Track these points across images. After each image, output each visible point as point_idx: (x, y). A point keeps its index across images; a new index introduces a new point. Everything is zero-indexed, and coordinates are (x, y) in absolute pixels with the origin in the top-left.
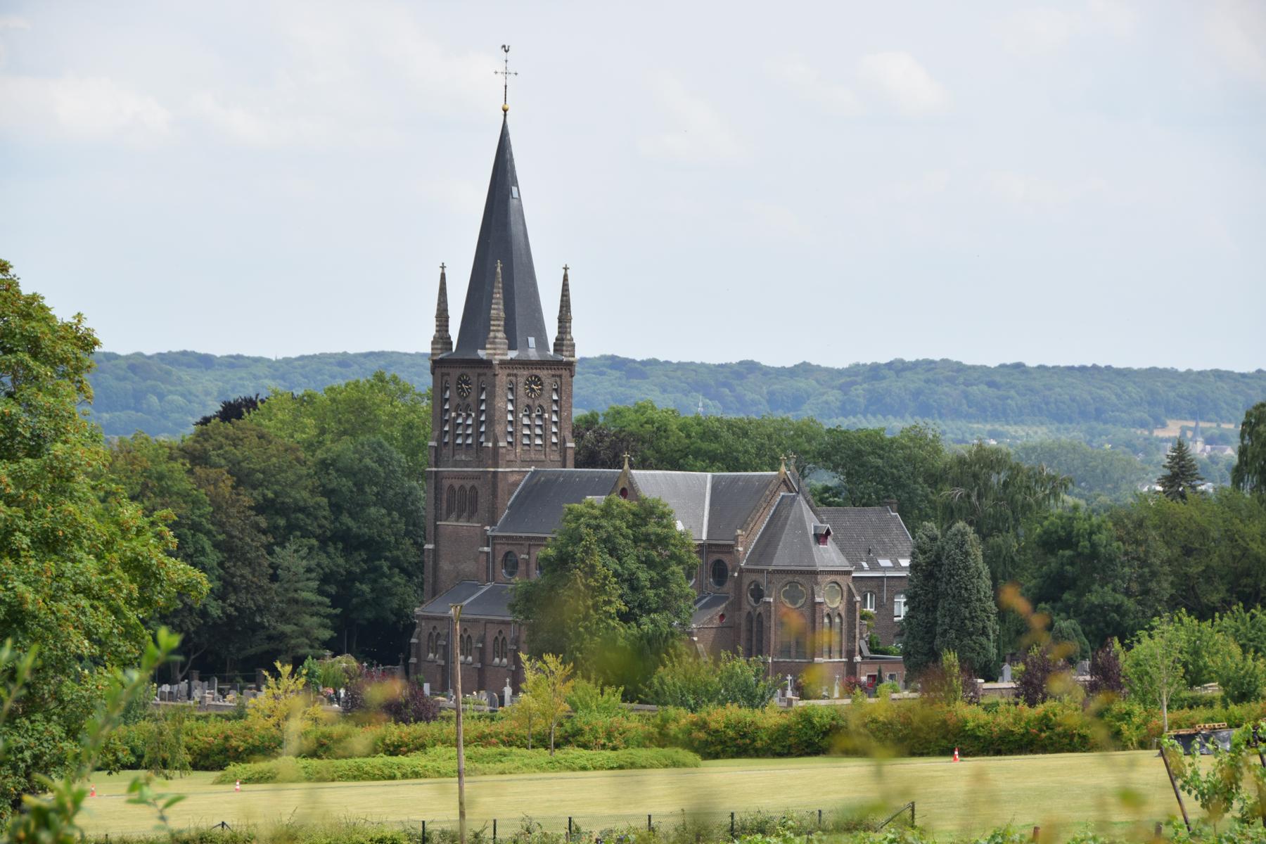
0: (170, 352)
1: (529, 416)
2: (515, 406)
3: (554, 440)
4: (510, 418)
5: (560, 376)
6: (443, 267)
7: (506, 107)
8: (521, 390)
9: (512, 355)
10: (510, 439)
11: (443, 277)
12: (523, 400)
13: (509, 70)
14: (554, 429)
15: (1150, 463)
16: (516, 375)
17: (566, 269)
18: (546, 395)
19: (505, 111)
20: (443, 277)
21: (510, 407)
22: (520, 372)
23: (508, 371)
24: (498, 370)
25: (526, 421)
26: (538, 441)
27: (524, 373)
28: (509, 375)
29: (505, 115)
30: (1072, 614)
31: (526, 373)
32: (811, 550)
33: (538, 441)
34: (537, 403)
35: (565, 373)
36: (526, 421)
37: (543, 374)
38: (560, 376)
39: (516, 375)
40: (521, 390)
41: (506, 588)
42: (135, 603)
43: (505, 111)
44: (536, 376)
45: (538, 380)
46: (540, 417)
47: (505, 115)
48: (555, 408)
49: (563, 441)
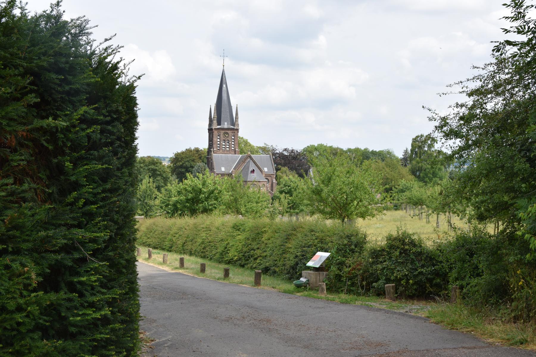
0: (137, 124)
1: (225, 142)
2: (220, 140)
3: (233, 149)
4: (218, 143)
8: (222, 136)
9: (219, 127)
10: (218, 148)
12: (222, 138)
13: (223, 57)
14: (233, 146)
15: (451, 264)
20: (237, 107)
21: (218, 140)
22: (221, 131)
24: (214, 131)
26: (228, 149)
30: (48, 289)
31: (223, 131)
32: (248, 175)
33: (228, 149)
34: (227, 139)
35: (236, 132)
36: (224, 144)
37: (229, 132)
40: (222, 136)
41: (19, 165)
42: (293, 190)
45: (227, 133)
46: (228, 143)
48: (233, 140)
49: (235, 149)
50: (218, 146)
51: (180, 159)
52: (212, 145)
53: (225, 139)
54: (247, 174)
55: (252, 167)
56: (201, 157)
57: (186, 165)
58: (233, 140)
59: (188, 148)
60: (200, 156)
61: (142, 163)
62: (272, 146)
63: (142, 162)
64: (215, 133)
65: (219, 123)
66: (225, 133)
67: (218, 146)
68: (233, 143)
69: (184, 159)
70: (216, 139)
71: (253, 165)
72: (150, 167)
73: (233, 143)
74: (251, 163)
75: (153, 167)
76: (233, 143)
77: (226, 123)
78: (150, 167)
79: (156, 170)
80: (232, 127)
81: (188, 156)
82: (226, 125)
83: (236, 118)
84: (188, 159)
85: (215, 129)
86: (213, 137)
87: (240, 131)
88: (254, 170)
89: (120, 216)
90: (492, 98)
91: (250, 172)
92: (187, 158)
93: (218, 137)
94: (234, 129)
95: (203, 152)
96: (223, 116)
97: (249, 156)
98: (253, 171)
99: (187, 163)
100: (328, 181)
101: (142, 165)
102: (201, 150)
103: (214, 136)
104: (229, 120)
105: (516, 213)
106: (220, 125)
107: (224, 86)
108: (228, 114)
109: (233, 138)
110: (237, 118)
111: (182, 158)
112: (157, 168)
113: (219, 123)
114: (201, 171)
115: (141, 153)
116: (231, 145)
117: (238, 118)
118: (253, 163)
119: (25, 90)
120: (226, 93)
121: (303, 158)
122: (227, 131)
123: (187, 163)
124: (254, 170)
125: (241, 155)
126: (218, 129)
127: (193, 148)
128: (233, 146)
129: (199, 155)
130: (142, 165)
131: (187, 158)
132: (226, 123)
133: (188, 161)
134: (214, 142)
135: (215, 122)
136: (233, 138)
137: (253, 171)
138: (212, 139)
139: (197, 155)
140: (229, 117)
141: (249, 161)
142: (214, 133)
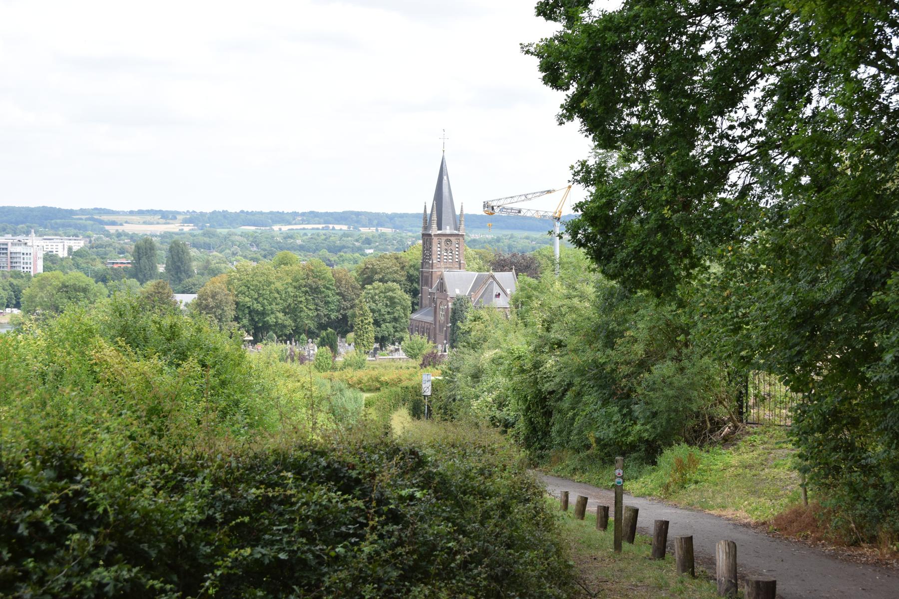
8: (443, 244)
9: (439, 232)
12: (444, 247)
18: (453, 245)
21: (439, 249)
24: (433, 237)
25: (445, 254)
27: (445, 238)
36: (445, 254)
37: (452, 238)
40: (443, 244)
45: (450, 241)
54: (491, 299)
55: (496, 290)
64: (435, 240)
65: (440, 228)
70: (435, 248)
71: (498, 287)
75: (390, 294)
76: (457, 253)
77: (448, 227)
79: (394, 298)
80: (456, 232)
82: (448, 230)
85: (435, 235)
88: (499, 294)
90: (835, 298)
91: (494, 296)
94: (458, 235)
96: (444, 209)
98: (498, 295)
100: (881, 378)
105: (407, 330)
107: (445, 178)
119: (612, 518)
124: (499, 294)
126: (439, 235)
132: (448, 227)
134: (433, 252)
137: (498, 295)
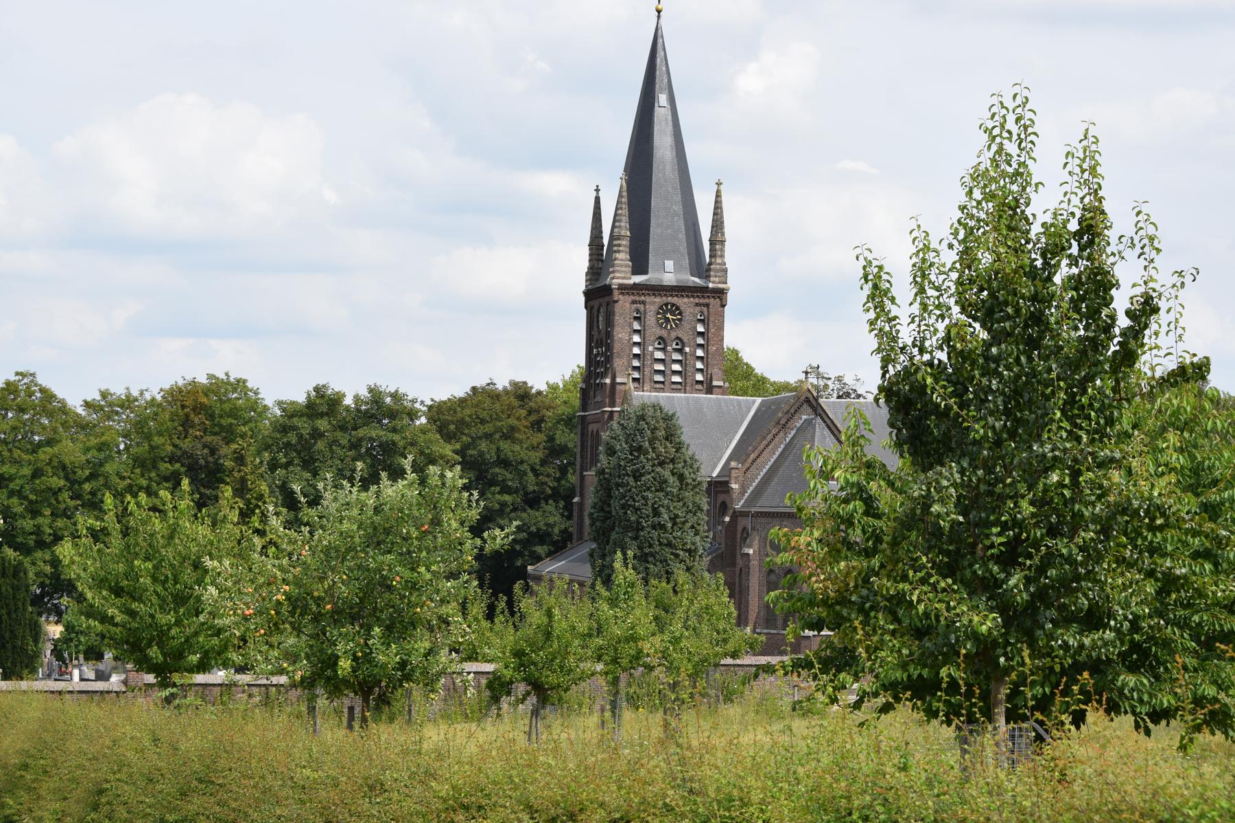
1: (664, 350)
3: (699, 377)
4: (636, 350)
5: (707, 305)
6: (597, 190)
7: (660, 7)
8: (651, 319)
11: (718, 195)
12: (654, 330)
14: (699, 365)
16: (644, 303)
17: (719, 184)
19: (659, 11)
20: (718, 195)
22: (648, 299)
23: (632, 298)
24: (616, 295)
26: (676, 379)
28: (634, 302)
29: (659, 17)
31: (658, 300)
33: (676, 379)
34: (673, 335)
35: (714, 302)
36: (659, 355)
37: (683, 302)
38: (707, 305)
39: (644, 303)
40: (651, 319)
43: (659, 11)
44: (673, 305)
45: (676, 309)
46: (680, 351)
47: (659, 17)
48: (700, 341)
50: (636, 363)
51: (452, 427)
52: (609, 359)
53: (664, 333)
56: (541, 420)
57: (481, 454)
58: (700, 341)
59: (481, 382)
60: (533, 418)
61: (322, 415)
62: (839, 379)
63: (325, 409)
64: (624, 305)
65: (640, 265)
66: (664, 309)
67: (636, 363)
68: (700, 353)
69: (468, 426)
70: (625, 334)
72: (361, 432)
73: (700, 353)
74: (820, 428)
77: (669, 264)
78: (361, 432)
81: (484, 415)
82: (668, 272)
83: (712, 243)
84: (488, 428)
85: (624, 289)
86: (609, 322)
87: (730, 297)
89: (1181, 450)
92: (483, 422)
93: (636, 326)
94: (703, 290)
95: (547, 401)
96: (655, 230)
97: (807, 401)
99: (483, 445)
101: (322, 424)
102: (539, 393)
103: (618, 319)
104: (683, 248)
106: (646, 272)
107: (662, 99)
108: (681, 224)
109: (700, 328)
110: (717, 240)
111: (462, 423)
112: (396, 438)
113: (640, 265)
114: (651, 442)
115: (269, 402)
116: (690, 360)
117: (723, 242)
118: (827, 432)
120: (670, 129)
121: (352, 608)
122: (675, 300)
123: (483, 445)
125: (759, 400)
126: (636, 287)
127: (502, 383)
128: (699, 365)
129: (530, 413)
130: (322, 424)
131: (483, 422)
132: (669, 264)
133: (488, 436)
134: (617, 347)
135: (622, 257)
136: (700, 328)
138: (609, 335)
139: (523, 413)
140: (682, 236)
141: (808, 423)
142: (618, 308)
